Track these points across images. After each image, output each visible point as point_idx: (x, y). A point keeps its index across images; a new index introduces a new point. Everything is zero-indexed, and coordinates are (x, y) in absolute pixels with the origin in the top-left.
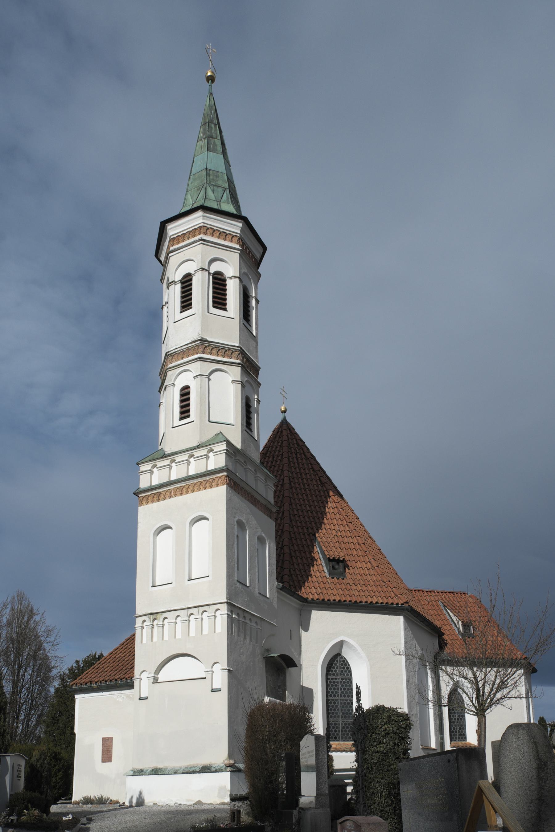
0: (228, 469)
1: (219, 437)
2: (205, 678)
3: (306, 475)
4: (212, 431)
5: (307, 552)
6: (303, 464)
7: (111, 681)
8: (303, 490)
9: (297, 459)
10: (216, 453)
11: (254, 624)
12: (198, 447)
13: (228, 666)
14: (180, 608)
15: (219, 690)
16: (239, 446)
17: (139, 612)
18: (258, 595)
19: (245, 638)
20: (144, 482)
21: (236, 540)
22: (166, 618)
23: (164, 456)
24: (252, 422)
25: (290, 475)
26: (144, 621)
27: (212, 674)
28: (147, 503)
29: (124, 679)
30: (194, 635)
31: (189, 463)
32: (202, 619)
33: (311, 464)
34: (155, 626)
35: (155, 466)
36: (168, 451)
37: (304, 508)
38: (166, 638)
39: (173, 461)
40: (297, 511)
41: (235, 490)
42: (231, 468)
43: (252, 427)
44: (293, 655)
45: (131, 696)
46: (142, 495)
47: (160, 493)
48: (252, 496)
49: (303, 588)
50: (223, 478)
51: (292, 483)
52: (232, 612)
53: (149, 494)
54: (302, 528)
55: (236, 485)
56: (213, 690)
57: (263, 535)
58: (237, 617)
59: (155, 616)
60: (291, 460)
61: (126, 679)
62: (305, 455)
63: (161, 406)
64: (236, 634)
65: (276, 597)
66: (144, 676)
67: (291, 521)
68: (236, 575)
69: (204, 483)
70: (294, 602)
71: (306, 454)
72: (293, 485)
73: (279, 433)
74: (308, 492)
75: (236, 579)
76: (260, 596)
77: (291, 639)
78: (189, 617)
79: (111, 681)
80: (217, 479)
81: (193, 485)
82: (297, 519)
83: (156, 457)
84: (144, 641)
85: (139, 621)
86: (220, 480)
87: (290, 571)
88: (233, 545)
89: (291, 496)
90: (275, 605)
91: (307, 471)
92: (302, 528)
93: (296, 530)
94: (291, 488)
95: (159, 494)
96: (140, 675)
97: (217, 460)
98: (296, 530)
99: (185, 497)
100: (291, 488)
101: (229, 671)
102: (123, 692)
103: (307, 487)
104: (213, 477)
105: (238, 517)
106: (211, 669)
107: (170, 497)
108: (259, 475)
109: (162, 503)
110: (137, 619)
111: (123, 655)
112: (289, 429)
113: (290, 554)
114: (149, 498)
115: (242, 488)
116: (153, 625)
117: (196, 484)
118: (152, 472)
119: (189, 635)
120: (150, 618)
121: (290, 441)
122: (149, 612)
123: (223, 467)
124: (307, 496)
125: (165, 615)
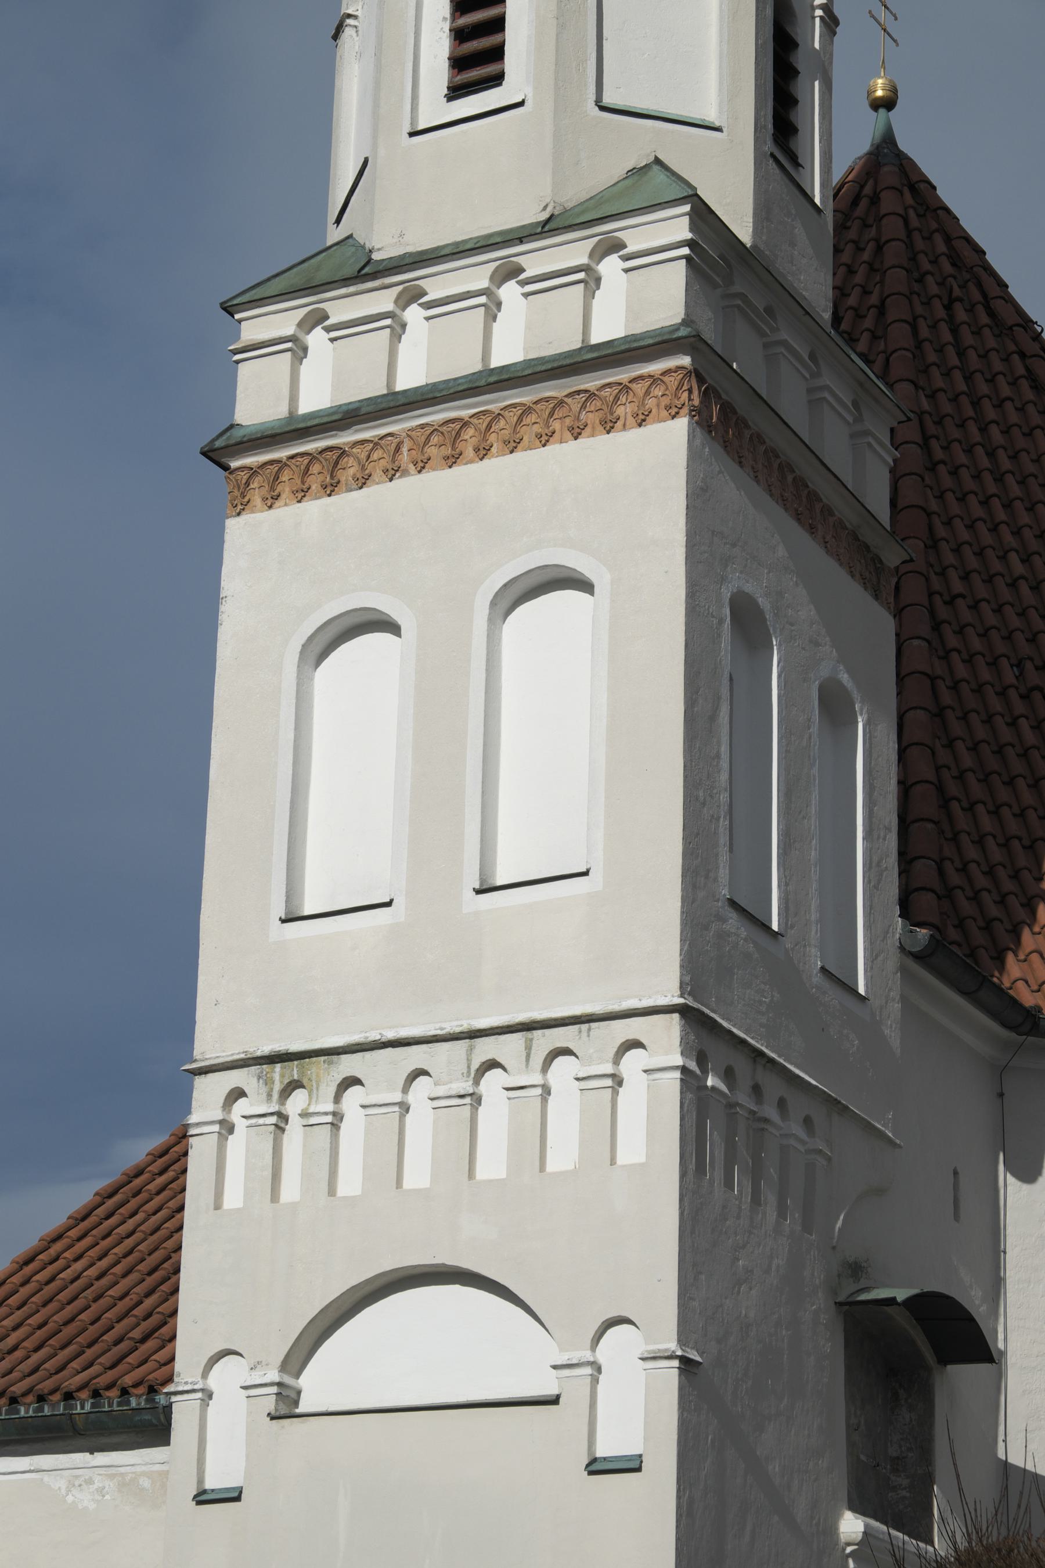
0: (698, 336)
1: (652, 185)
2: (555, 1401)
3: (999, 405)
4: (612, 154)
5: (1021, 783)
6: (984, 356)
7: (41, 1399)
8: (987, 477)
9: (954, 331)
10: (637, 262)
11: (799, 1131)
12: (549, 227)
13: (682, 1341)
14: (431, 1030)
15: (632, 1466)
16: (744, 230)
17: (211, 1041)
18: (817, 979)
19: (756, 1199)
20: (259, 397)
21: (725, 692)
22: (353, 1081)
23: (367, 271)
24: (798, 117)
25: (926, 405)
26: (237, 1094)
27: (595, 1381)
28: (272, 500)
29: (114, 1393)
30: (358, 1192)
31: (493, 308)
32: (547, 1091)
33: (1023, 355)
34: (295, 1126)
35: (317, 319)
36: (386, 245)
37: (997, 566)
38: (350, 1183)
39: (412, 296)
40: (965, 577)
41: (726, 445)
42: (709, 335)
43: (798, 145)
44: (974, 1301)
45: (145, 1483)
46: (249, 463)
47: (342, 452)
48: (800, 483)
49: (1010, 958)
50: (672, 381)
51: (934, 444)
52: (702, 1059)
53: (282, 453)
54: (994, 664)
55: (733, 427)
56: (596, 1467)
57: (845, 678)
58: (723, 1087)
59: (294, 1071)
60: (924, 332)
61: (125, 1392)
62: (991, 313)
63: (348, 33)
64: (719, 1174)
65: (895, 994)
66: (226, 1379)
67: (937, 626)
68: (723, 874)
69: (574, 404)
70: (971, 1026)
71: (998, 305)
72: (939, 454)
73: (864, 203)
74: (1016, 490)
75: (725, 892)
76: (826, 984)
77: (957, 1217)
78: (477, 1082)
79: (41, 1399)
80: (639, 388)
81: (512, 416)
82: (967, 616)
83: (322, 276)
84: (233, 1198)
85: (207, 1097)
86: (658, 391)
87: (941, 872)
88: (713, 718)
89: (934, 505)
90: (892, 1033)
91: (1006, 391)
92: (994, 664)
93: (961, 671)
94: (933, 467)
95: (332, 456)
96: (205, 1375)
97: (641, 294)
98: (961, 671)
99: (471, 474)
100: (933, 467)
101: (686, 1363)
102: (102, 1458)
103: (1006, 464)
104: (623, 375)
105: (736, 582)
106: (588, 1356)
107: (393, 473)
108: (827, 379)
109: (348, 503)
110: (200, 1082)
111: (92, 1272)
112: (913, 188)
113: (940, 788)
114: (285, 476)
115: (758, 438)
116: (283, 1117)
117: (527, 410)
118: (300, 351)
119: (471, 1174)
120: (269, 1082)
121: (920, 244)
122: (266, 1049)
123: (676, 328)
124: (1008, 506)
125: (349, 1066)
